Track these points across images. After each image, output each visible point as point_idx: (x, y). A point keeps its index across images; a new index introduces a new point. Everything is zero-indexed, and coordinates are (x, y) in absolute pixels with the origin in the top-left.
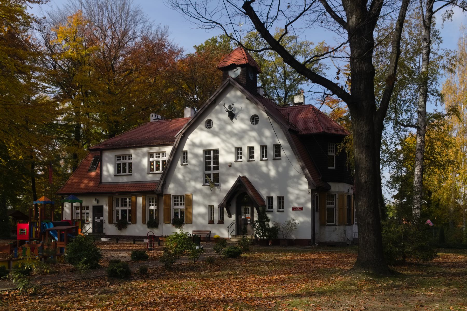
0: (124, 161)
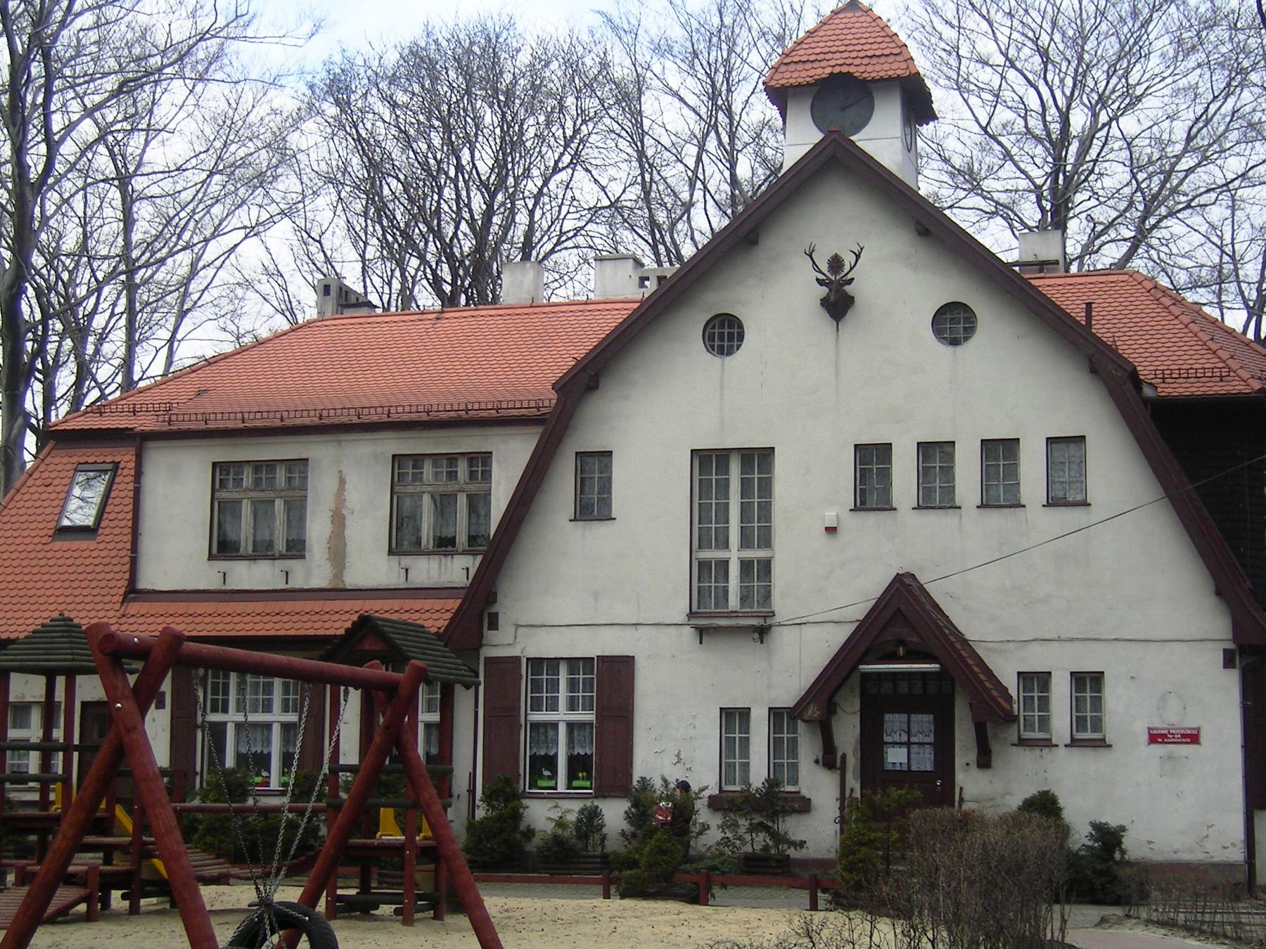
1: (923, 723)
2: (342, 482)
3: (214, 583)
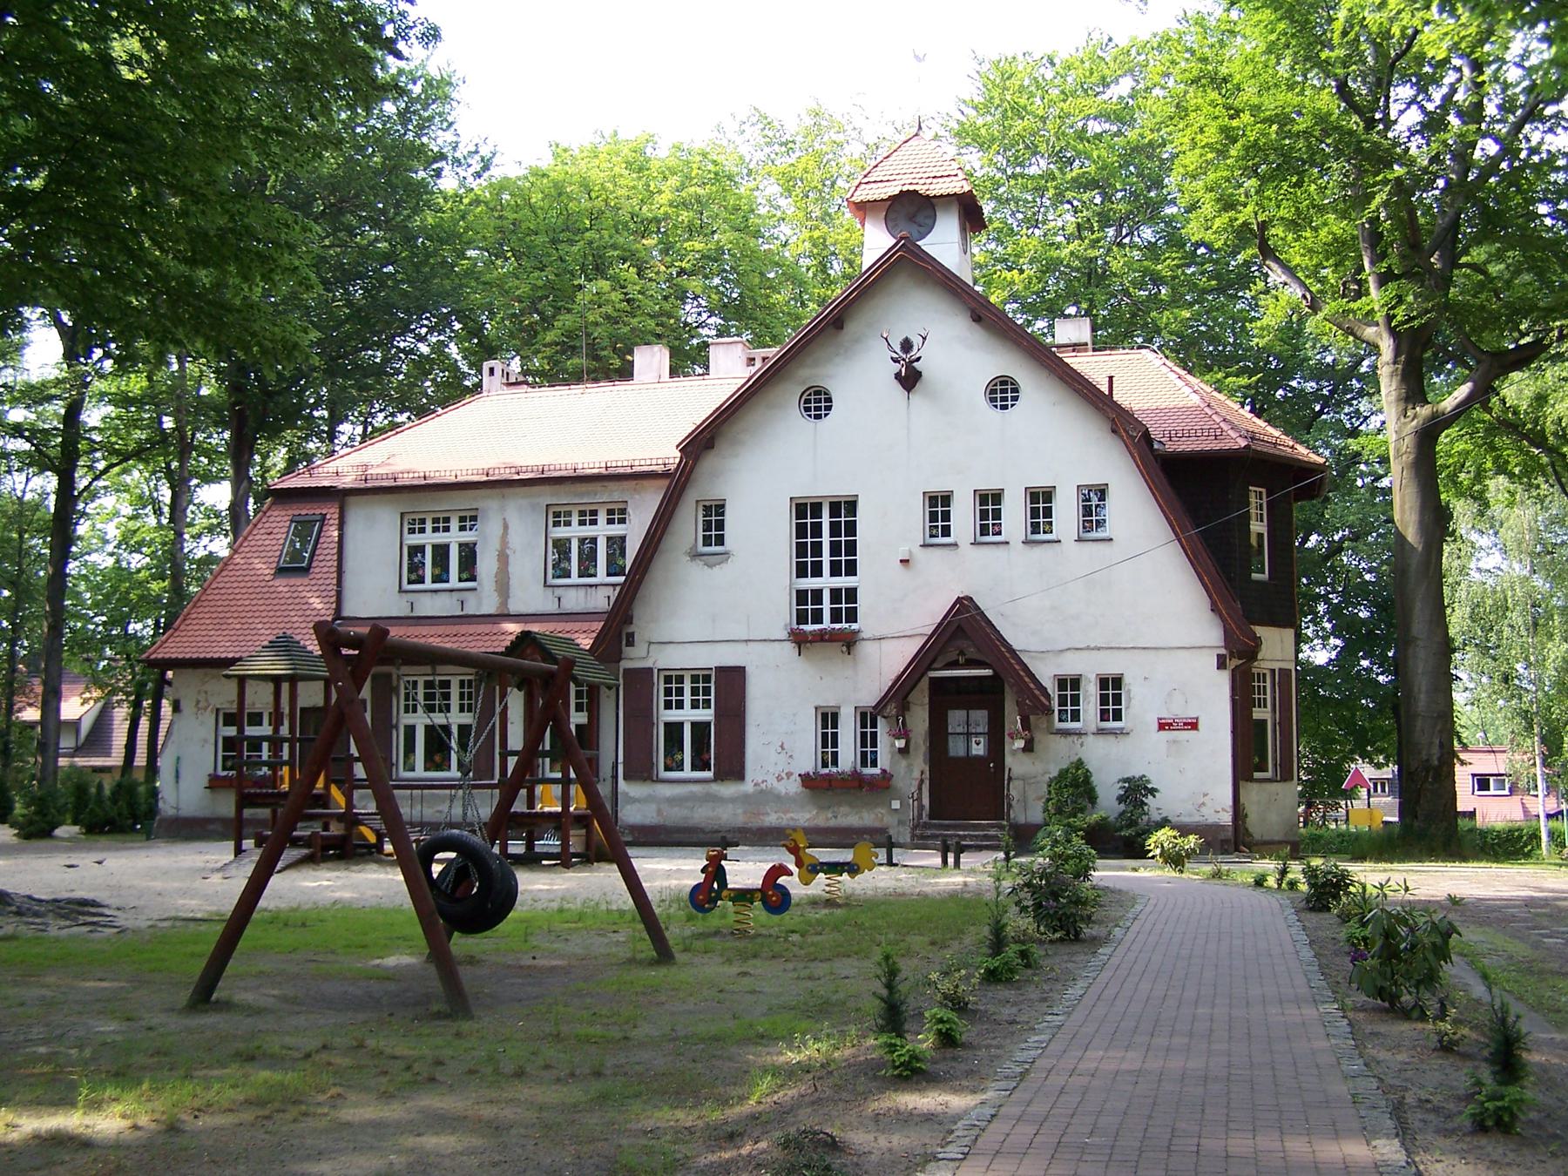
0: (440, 538)
1: (980, 717)
2: (506, 527)
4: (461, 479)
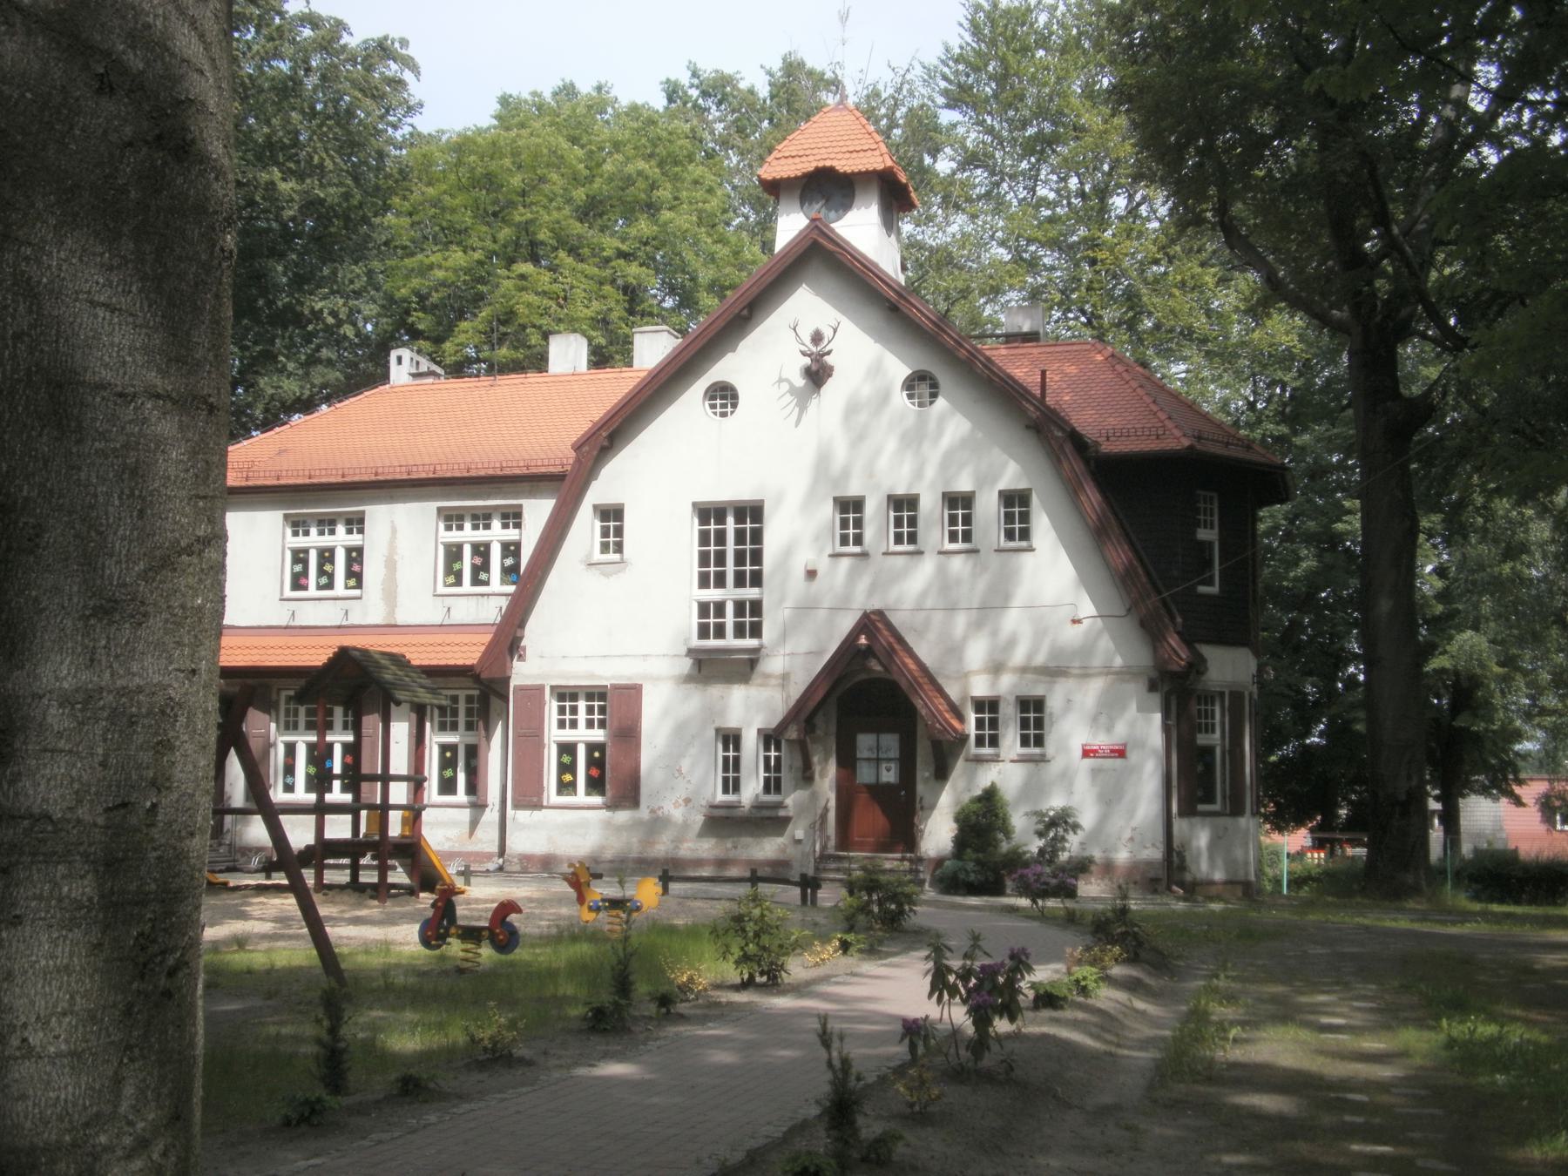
2: (394, 531)
3: (436, 617)
4: (507, 472)
